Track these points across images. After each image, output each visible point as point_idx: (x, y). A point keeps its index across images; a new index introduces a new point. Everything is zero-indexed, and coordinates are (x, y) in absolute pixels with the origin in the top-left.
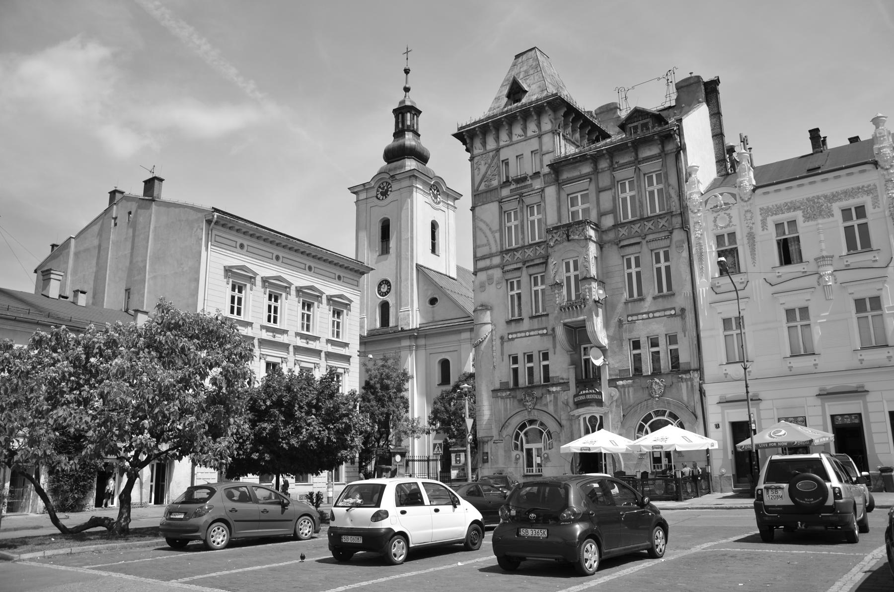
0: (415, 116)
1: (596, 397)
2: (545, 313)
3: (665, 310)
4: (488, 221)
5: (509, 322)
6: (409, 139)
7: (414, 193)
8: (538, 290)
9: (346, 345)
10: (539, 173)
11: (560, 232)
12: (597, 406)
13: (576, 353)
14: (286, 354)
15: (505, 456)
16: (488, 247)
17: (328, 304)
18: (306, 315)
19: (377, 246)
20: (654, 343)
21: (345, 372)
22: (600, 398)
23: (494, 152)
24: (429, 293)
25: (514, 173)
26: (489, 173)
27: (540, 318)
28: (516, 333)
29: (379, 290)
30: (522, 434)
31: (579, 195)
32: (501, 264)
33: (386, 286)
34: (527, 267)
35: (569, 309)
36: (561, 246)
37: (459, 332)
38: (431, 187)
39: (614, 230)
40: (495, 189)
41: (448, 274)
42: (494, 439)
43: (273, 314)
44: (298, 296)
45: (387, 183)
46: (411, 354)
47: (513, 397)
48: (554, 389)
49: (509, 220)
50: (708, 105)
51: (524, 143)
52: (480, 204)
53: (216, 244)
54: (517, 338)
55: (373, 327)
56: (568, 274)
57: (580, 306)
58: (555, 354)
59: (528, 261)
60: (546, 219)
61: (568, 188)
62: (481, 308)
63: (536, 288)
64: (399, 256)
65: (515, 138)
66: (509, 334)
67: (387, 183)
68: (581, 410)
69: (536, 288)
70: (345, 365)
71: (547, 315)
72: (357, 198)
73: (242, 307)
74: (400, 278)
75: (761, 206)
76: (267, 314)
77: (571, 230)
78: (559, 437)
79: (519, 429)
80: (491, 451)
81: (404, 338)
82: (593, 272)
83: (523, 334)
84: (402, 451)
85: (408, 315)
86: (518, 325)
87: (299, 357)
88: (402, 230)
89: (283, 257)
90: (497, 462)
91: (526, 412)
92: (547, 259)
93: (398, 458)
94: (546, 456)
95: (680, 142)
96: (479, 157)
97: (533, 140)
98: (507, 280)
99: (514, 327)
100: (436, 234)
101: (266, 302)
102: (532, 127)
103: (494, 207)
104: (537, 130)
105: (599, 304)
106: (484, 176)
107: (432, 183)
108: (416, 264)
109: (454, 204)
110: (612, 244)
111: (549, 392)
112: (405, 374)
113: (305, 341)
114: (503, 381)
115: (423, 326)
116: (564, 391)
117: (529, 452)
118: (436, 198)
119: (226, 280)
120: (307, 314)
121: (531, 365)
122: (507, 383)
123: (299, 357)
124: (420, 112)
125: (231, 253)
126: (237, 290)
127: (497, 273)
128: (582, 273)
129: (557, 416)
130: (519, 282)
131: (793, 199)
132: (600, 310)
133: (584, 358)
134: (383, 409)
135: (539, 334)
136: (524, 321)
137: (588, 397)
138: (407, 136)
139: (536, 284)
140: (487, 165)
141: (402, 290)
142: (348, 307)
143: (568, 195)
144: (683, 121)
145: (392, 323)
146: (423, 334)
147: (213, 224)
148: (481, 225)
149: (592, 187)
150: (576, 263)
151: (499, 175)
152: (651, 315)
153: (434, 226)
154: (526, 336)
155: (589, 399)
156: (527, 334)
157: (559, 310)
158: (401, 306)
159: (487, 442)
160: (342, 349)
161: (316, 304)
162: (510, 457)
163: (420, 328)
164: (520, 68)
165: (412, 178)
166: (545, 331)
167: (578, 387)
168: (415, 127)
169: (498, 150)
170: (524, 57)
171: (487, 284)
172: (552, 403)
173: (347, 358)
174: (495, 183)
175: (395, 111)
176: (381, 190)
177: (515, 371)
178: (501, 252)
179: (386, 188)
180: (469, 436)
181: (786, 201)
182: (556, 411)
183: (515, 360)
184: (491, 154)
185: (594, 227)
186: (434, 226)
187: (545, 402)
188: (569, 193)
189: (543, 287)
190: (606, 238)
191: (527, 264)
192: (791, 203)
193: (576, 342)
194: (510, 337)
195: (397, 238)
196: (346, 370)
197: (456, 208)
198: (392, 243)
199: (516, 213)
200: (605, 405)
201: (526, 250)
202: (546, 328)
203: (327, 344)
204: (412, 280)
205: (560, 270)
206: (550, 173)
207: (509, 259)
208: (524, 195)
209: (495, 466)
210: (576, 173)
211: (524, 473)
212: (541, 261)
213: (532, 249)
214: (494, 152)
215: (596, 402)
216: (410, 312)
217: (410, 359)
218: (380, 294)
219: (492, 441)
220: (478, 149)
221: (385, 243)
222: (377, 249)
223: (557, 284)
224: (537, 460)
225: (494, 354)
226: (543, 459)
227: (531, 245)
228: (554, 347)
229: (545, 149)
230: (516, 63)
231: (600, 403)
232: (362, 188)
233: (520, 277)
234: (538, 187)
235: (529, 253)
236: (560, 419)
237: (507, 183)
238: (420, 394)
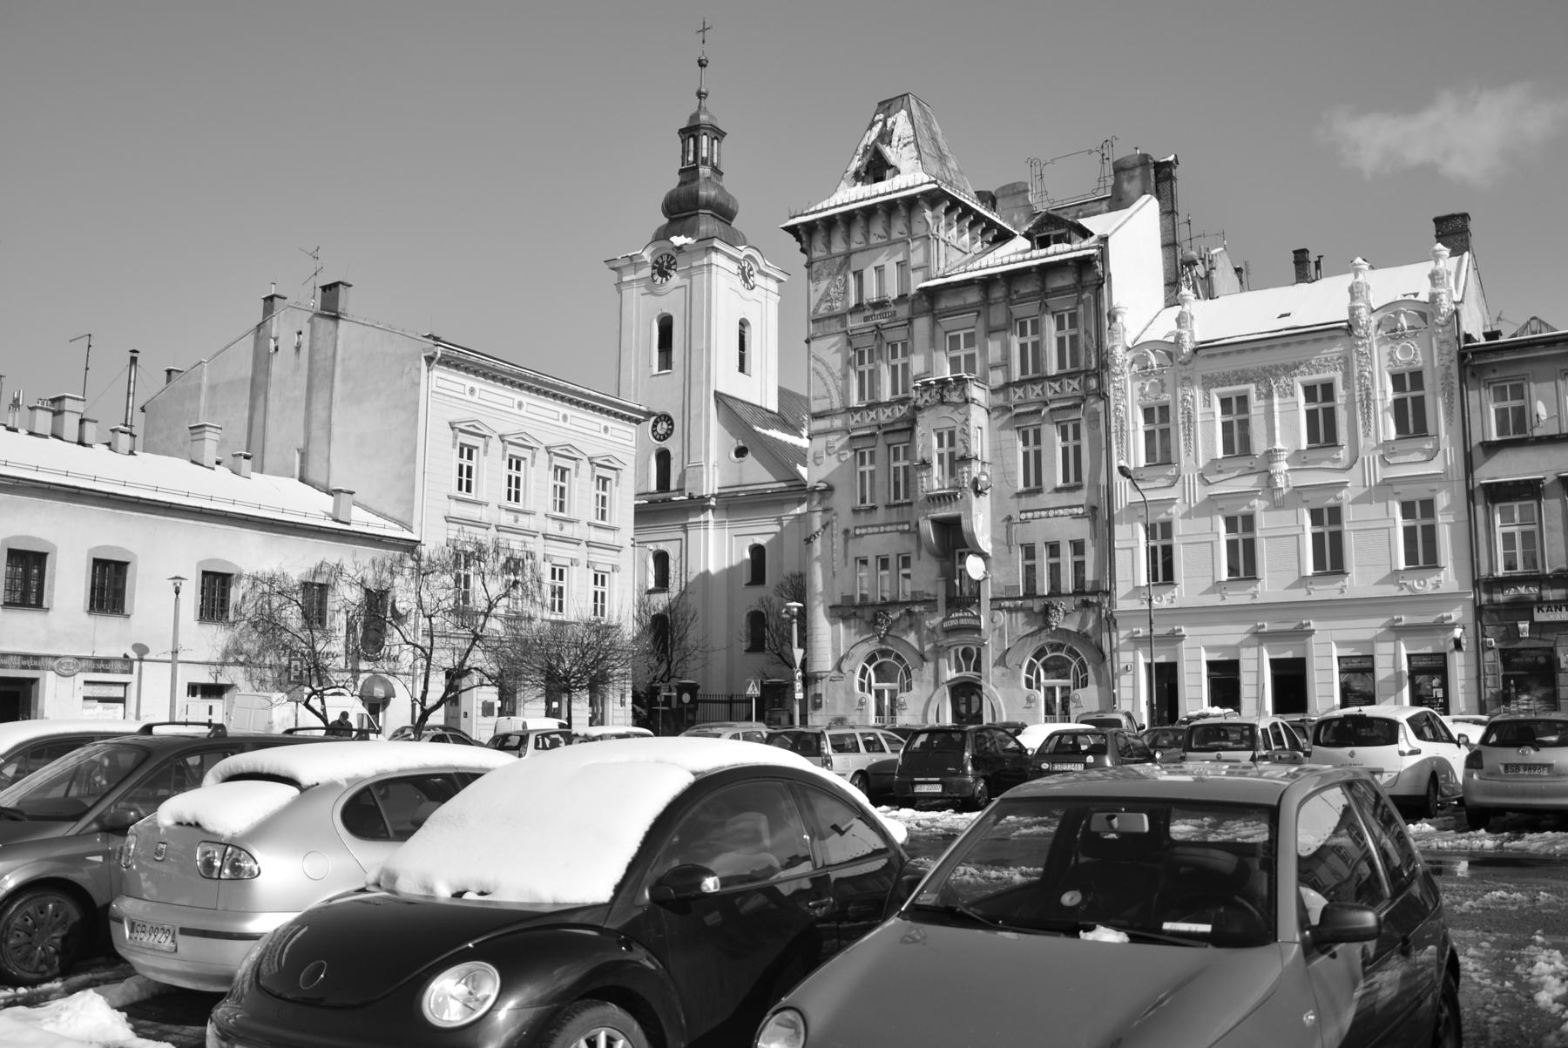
0: (716, 142)
1: (973, 622)
2: (908, 501)
3: (1071, 507)
5: (856, 511)
16: (828, 401)
20: (1054, 549)
22: (978, 623)
28: (866, 527)
30: (870, 670)
31: (962, 334)
34: (885, 433)
41: (764, 406)
43: (514, 489)
50: (1159, 199)
54: (867, 534)
58: (919, 559)
61: (947, 323)
65: (874, 240)
67: (668, 255)
69: (896, 464)
71: (910, 504)
75: (1204, 373)
76: (507, 488)
83: (876, 530)
85: (702, 473)
86: (869, 515)
90: (834, 707)
95: (1103, 272)
99: (863, 519)
101: (506, 471)
104: (906, 231)
108: (715, 392)
115: (723, 491)
124: (723, 134)
130: (872, 454)
131: (1246, 367)
135: (898, 531)
137: (963, 622)
139: (896, 459)
143: (946, 333)
144: (1110, 240)
147: (435, 362)
149: (981, 324)
152: (1051, 513)
156: (882, 529)
169: (847, 256)
173: (618, 549)
175: (682, 131)
181: (1236, 368)
184: (838, 260)
192: (1242, 371)
193: (948, 544)
194: (858, 532)
199: (871, 352)
202: (908, 523)
212: (905, 425)
214: (842, 258)
218: (655, 437)
219: (828, 678)
225: (835, 555)
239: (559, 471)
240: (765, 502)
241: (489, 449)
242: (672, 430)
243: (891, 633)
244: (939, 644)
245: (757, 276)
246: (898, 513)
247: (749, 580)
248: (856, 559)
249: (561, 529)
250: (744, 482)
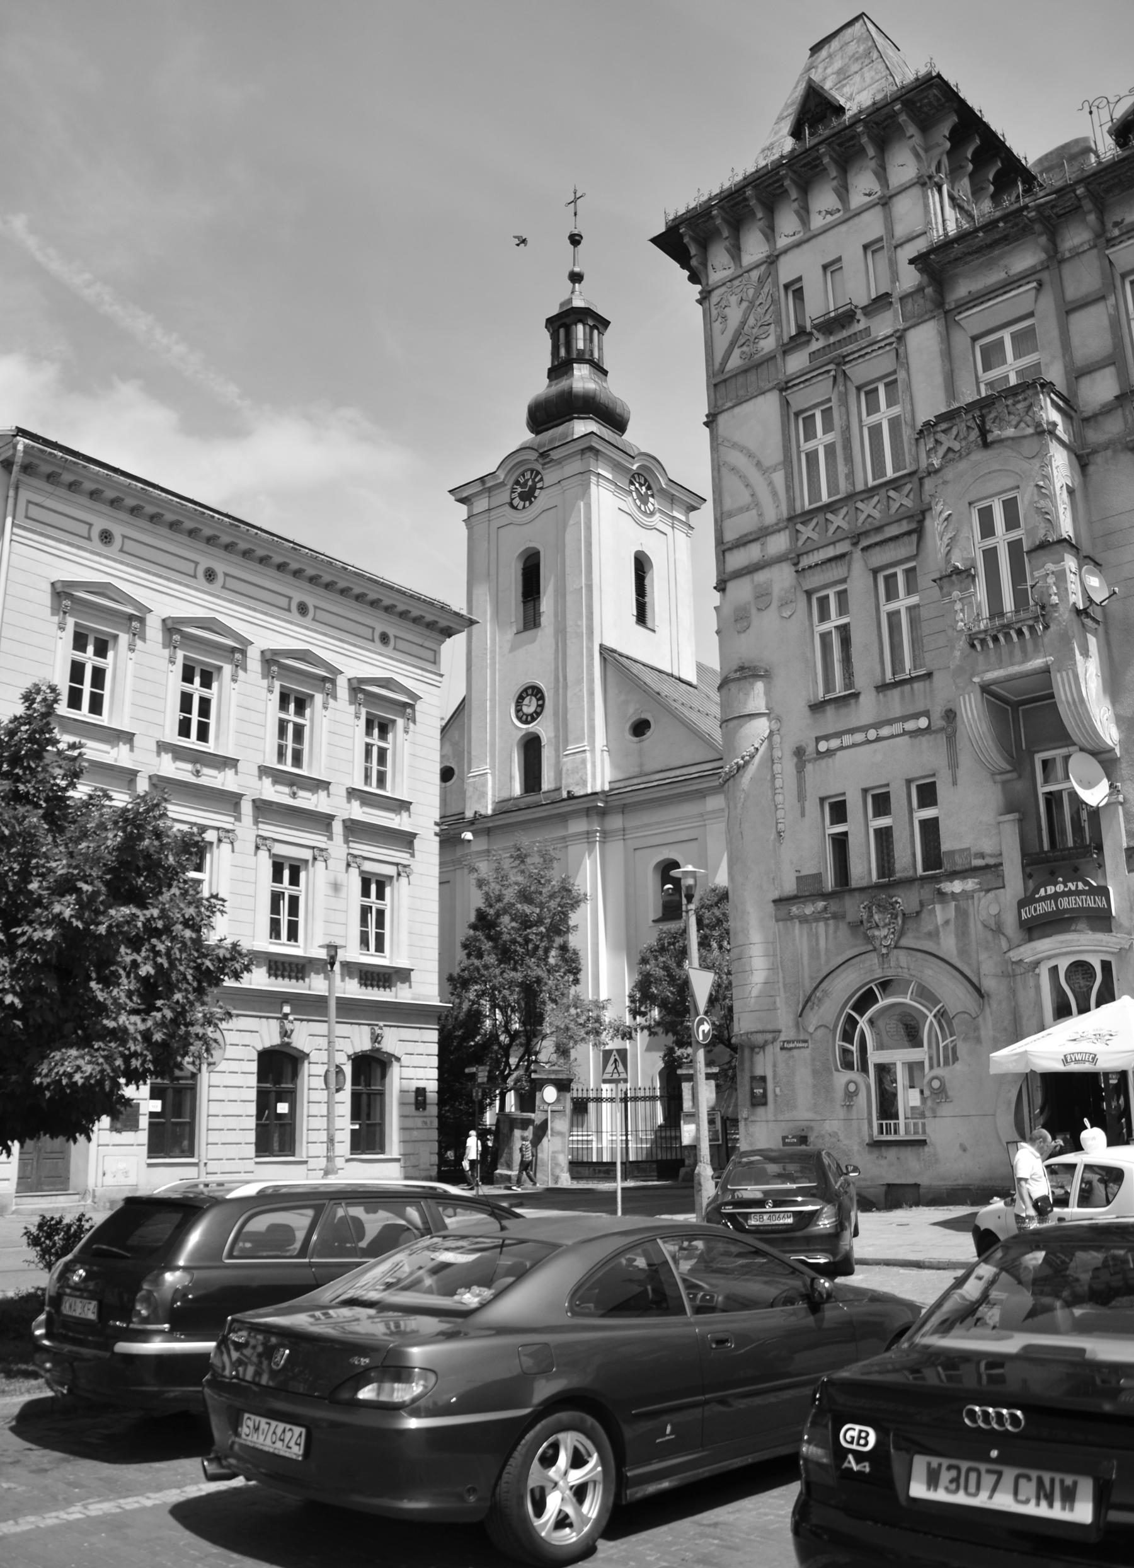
0: (596, 332)
1: (1090, 902)
4: (752, 446)
5: (817, 707)
6: (582, 379)
7: (593, 487)
8: (898, 612)
9: (403, 806)
10: (887, 295)
11: (960, 426)
12: (1094, 929)
13: (1020, 777)
14: (232, 820)
15: (815, 1086)
16: (754, 512)
17: (353, 701)
18: (290, 727)
19: (513, 612)
21: (399, 875)
22: (1102, 903)
23: (763, 268)
24: (631, 711)
25: (817, 305)
26: (751, 321)
27: (907, 688)
28: (838, 735)
29: (518, 710)
31: (1006, 335)
32: (790, 551)
33: (534, 699)
35: (995, 639)
36: (963, 465)
37: (702, 794)
38: (634, 477)
39: (1120, 411)
40: (771, 358)
41: (676, 674)
42: (783, 1037)
44: (267, 674)
46: (591, 851)
47: (835, 916)
48: (957, 886)
49: (810, 435)
51: (843, 228)
52: (729, 404)
53: (28, 524)
54: (842, 748)
55: (505, 795)
56: (989, 543)
57: (1032, 628)
58: (955, 783)
59: (866, 533)
60: (913, 411)
61: (974, 320)
62: (738, 675)
63: (892, 606)
64: (561, 631)
65: (817, 222)
66: (818, 739)
67: (532, 471)
68: (1044, 946)
69: (892, 606)
70: (401, 857)
72: (469, 511)
73: (107, 693)
74: (565, 679)
76: (178, 715)
77: (992, 415)
78: (977, 1029)
79: (854, 1008)
80: (775, 1071)
81: (574, 814)
82: (1066, 527)
83: (859, 737)
84: (560, 1076)
85: (584, 762)
86: (844, 711)
87: (268, 830)
88: (568, 570)
89: (226, 575)
91: (874, 959)
92: (921, 522)
93: (550, 1093)
94: (936, 1084)
96: (723, 289)
97: (866, 216)
98: (809, 594)
99: (832, 720)
100: (647, 582)
101: (174, 685)
102: (864, 184)
103: (767, 407)
105: (1088, 622)
106: (738, 334)
107: (635, 467)
108: (601, 646)
109: (687, 518)
110: (1115, 452)
111: (940, 893)
112: (566, 889)
113: (286, 790)
114: (804, 873)
116: (988, 891)
117: (884, 1070)
118: (646, 503)
119: (56, 619)
120: (296, 725)
121: (883, 822)
122: (818, 877)
123: (268, 830)
124: (606, 323)
125: (74, 550)
126: (90, 649)
127: (781, 577)
128: (1030, 532)
129: (969, 965)
130: (842, 596)
132: (1092, 641)
133: (1042, 789)
134: (513, 974)
135: (905, 733)
136: (862, 698)
137: (1065, 903)
138: (576, 372)
140: (745, 304)
141: (569, 705)
142: (409, 711)
143: (974, 339)
145: (546, 785)
146: (617, 803)
148: (735, 458)
149: (1047, 305)
150: (1010, 507)
151: (778, 322)
153: (641, 565)
154: (869, 742)
155: (1066, 911)
156: (872, 734)
157: (967, 647)
158: (566, 742)
159: (763, 1047)
160: (391, 815)
161: (319, 698)
162: (828, 1089)
163: (611, 790)
164: (825, 69)
165: (589, 454)
166: (923, 723)
167: (1030, 876)
168: (596, 355)
169: (772, 260)
170: (835, 44)
171: (754, 611)
172: (952, 927)
173: (406, 840)
174: (768, 344)
175: (550, 322)
176: (519, 490)
177: (840, 843)
178: (791, 519)
179: (530, 483)
180: (701, 1022)
182: (963, 952)
183: (839, 811)
184: (755, 275)
185: (1061, 403)
186: (641, 565)
187: (931, 928)
188: (975, 332)
189: (914, 600)
190: (1094, 436)
191: (865, 543)
194: (823, 746)
195: (556, 590)
196: (403, 870)
197: (691, 528)
198: (546, 604)
199: (827, 413)
200: (1121, 925)
201: (860, 505)
202: (926, 714)
203: (349, 801)
204: (591, 681)
205: (965, 532)
206: (920, 289)
207: (815, 536)
208: (847, 359)
209: (787, 1116)
210: (995, 277)
211: (871, 1136)
212: (905, 527)
213: (876, 499)
215: (1088, 918)
216: (588, 754)
217: (588, 862)
218: (520, 719)
219: (778, 1045)
220: (720, 266)
221: (531, 604)
222: (513, 620)
223: (957, 571)
224: (908, 1099)
226: (927, 1093)
227: (871, 492)
228: (953, 765)
229: (900, 231)
230: (811, 63)
231: (1102, 920)
232: (478, 488)
233: (844, 581)
234: (888, 331)
235: (870, 509)
236: (979, 974)
237: (802, 336)
238: (613, 947)
240: (679, 795)
243: (904, 942)
246: (902, 697)
247: (660, 915)
249: (980, 1278)
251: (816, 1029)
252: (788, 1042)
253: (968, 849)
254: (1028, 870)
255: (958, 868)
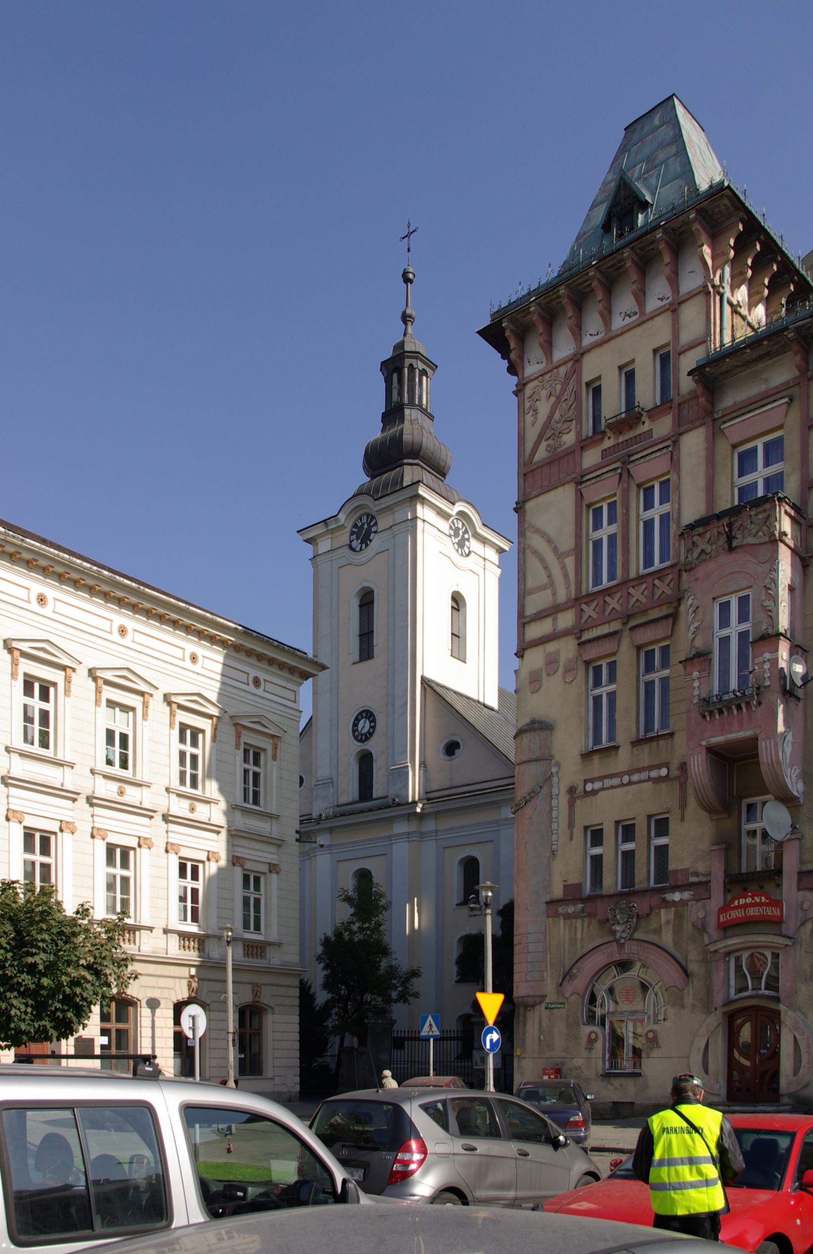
0: (424, 378)
1: (770, 911)
23: (570, 364)
26: (557, 416)
28: (601, 778)
31: (759, 444)
41: (481, 700)
45: (368, 515)
48: (677, 896)
54: (603, 789)
58: (683, 819)
61: (735, 429)
65: (618, 323)
67: (368, 515)
78: (682, 998)
83: (616, 781)
91: (614, 947)
99: (597, 767)
127: (567, 649)
135: (650, 779)
137: (751, 912)
140: (553, 399)
143: (734, 447)
148: (536, 541)
154: (622, 785)
156: (626, 779)
159: (533, 1006)
166: (664, 772)
169: (577, 359)
172: (671, 926)
175: (384, 364)
179: (366, 526)
184: (562, 370)
194: (589, 787)
202: (667, 765)
214: (570, 364)
232: (320, 529)
239: (188, 732)
241: (73, 688)
242: (374, 728)
244: (712, 948)
245: (472, 540)
248: (586, 828)
250: (456, 783)
251: (571, 995)
252: (551, 1004)
253: (687, 870)
254: (728, 887)
255: (679, 883)
